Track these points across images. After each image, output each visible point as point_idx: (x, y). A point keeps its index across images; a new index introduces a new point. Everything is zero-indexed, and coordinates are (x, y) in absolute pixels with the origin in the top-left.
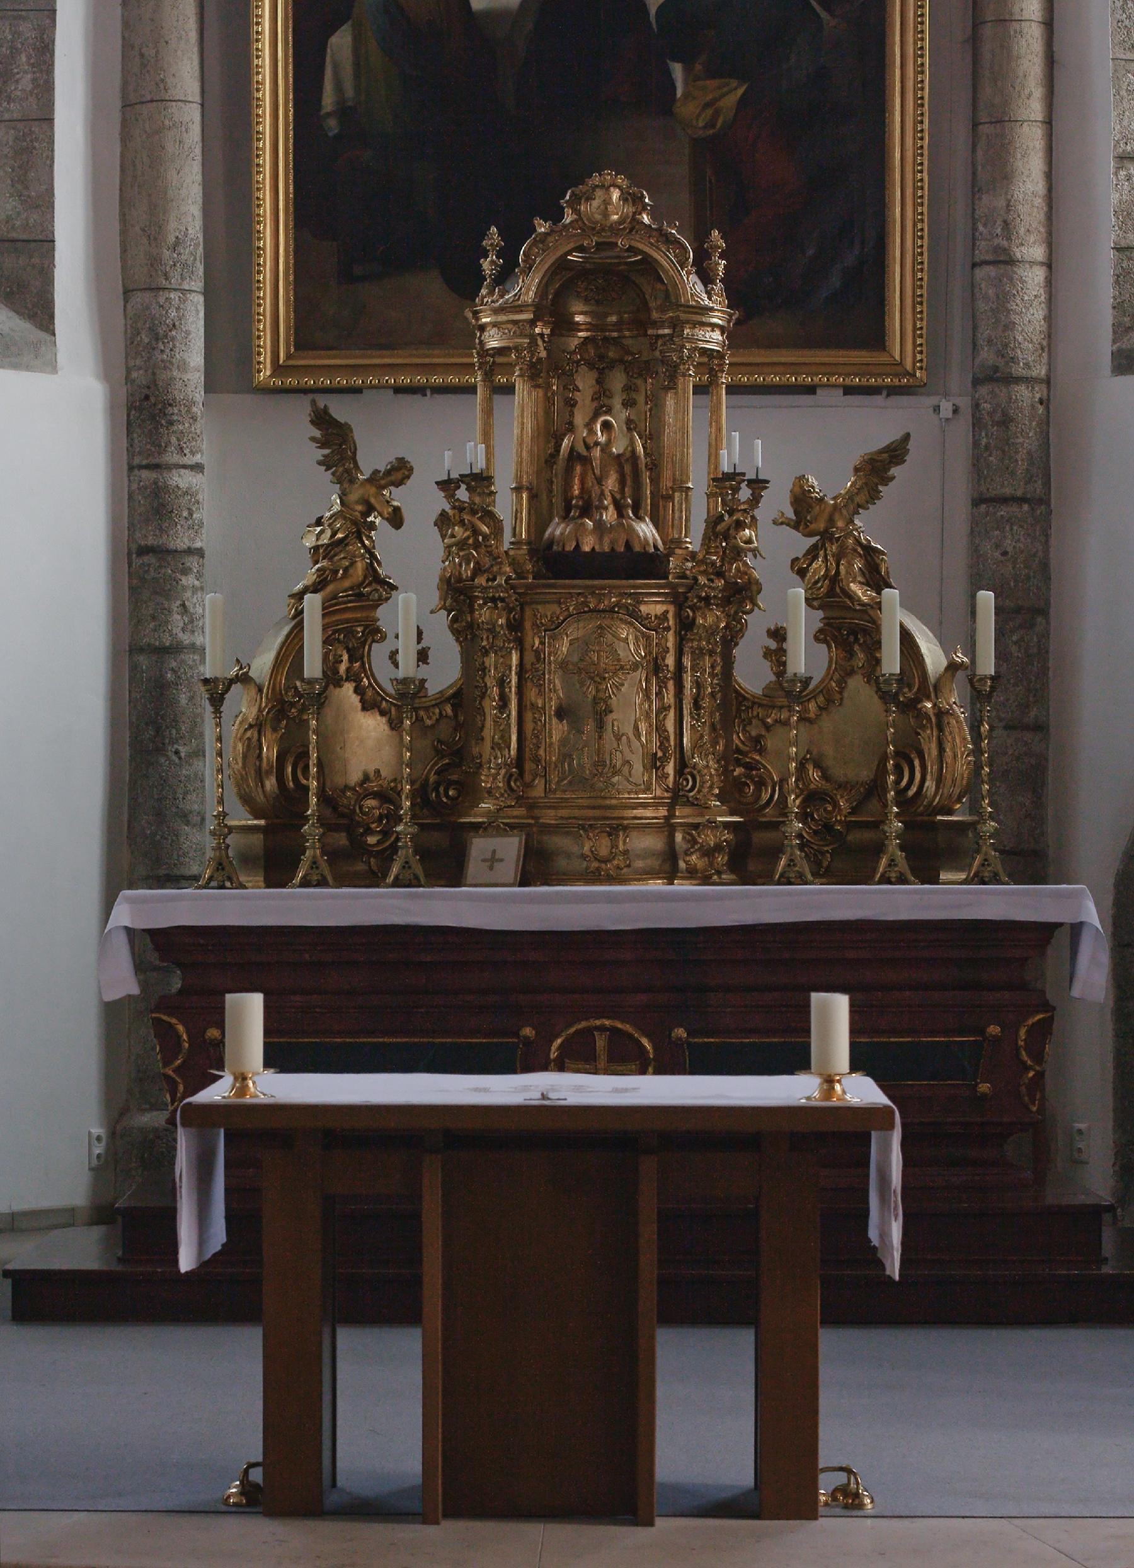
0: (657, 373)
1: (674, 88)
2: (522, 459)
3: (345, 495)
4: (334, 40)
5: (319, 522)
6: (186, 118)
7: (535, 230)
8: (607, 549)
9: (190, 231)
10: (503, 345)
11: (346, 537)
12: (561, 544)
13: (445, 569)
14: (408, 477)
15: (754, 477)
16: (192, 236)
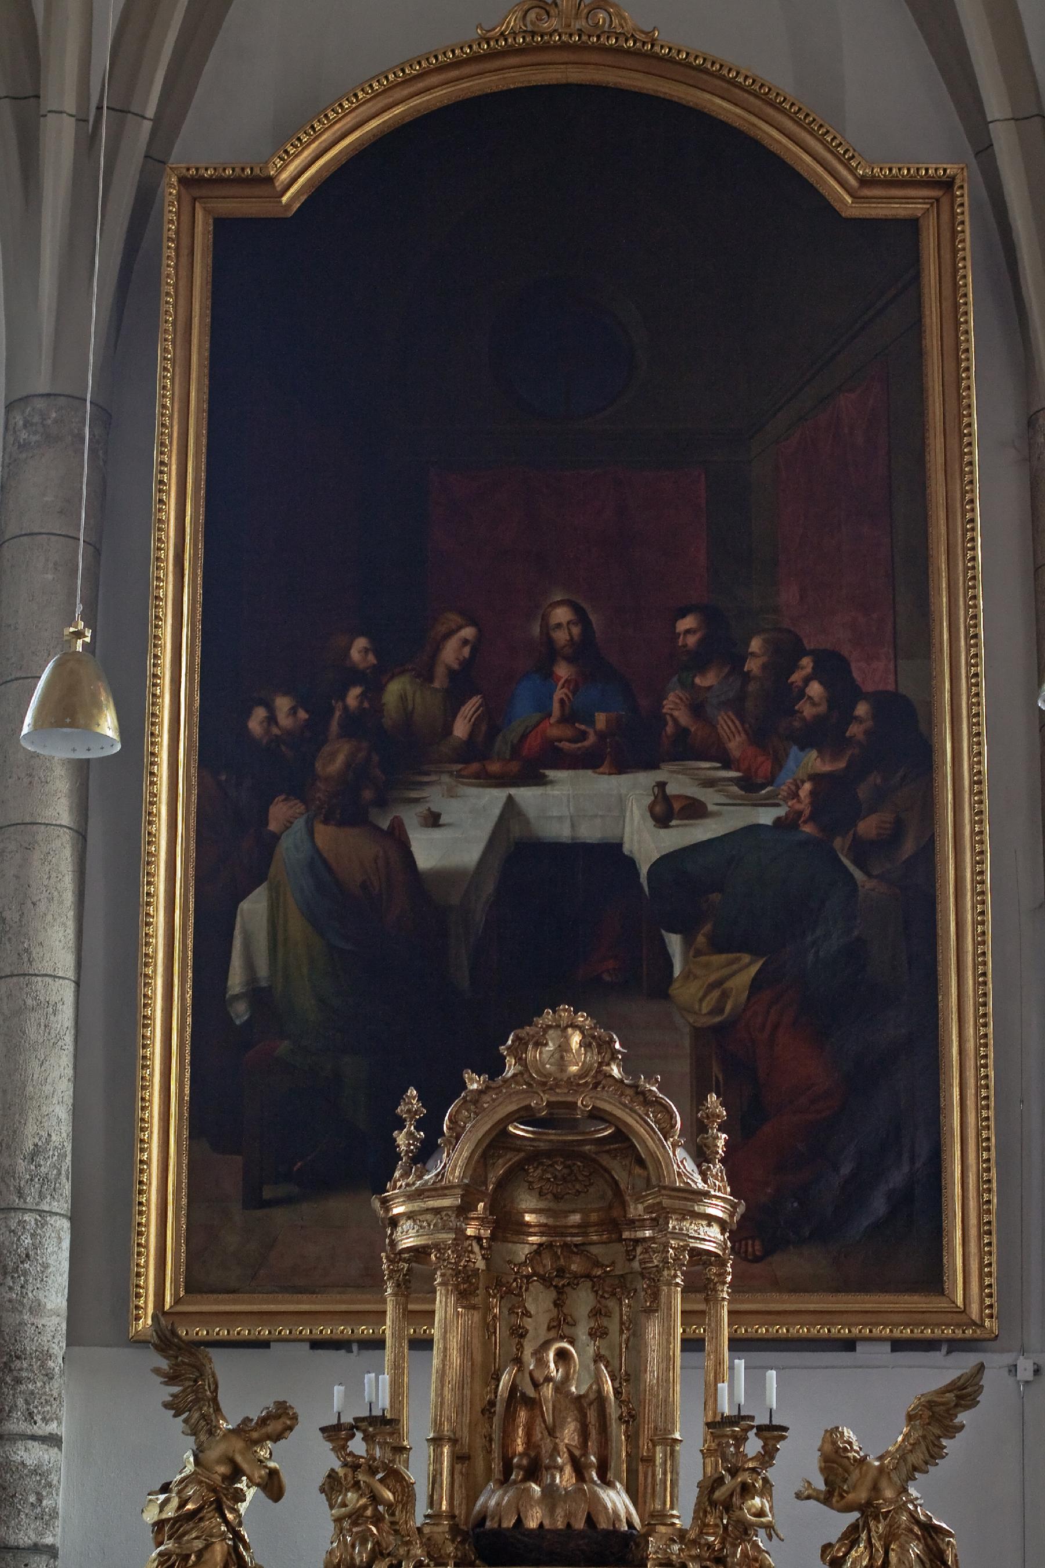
0: (636, 1291)
1: (670, 966)
2: (443, 1399)
3: (201, 1451)
4: (245, 905)
5: (165, 1488)
6: (54, 998)
7: (465, 1087)
8: (560, 1525)
9: (54, 1138)
10: (423, 1242)
11: (199, 1510)
12: (496, 1519)
13: (331, 1553)
14: (290, 1428)
15: (767, 1422)
16: (57, 1144)
